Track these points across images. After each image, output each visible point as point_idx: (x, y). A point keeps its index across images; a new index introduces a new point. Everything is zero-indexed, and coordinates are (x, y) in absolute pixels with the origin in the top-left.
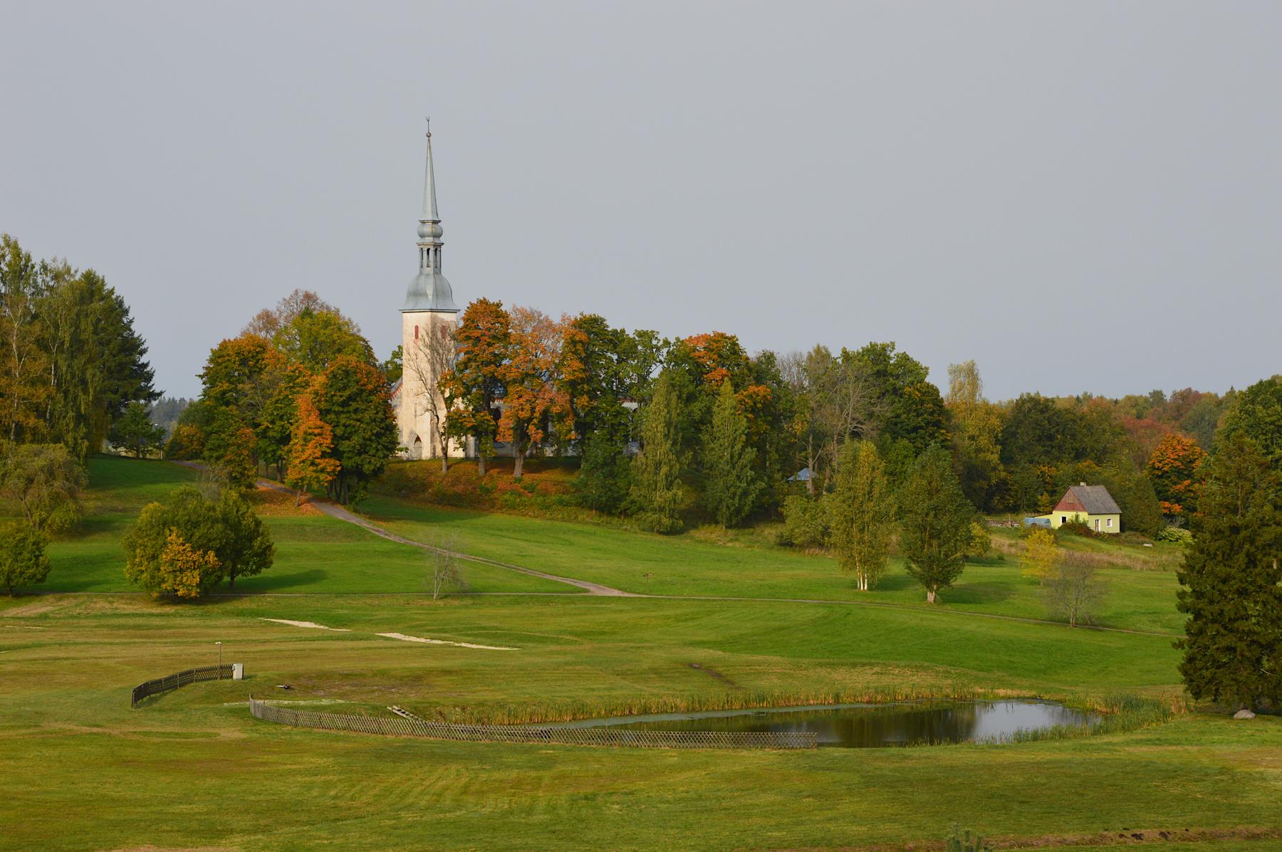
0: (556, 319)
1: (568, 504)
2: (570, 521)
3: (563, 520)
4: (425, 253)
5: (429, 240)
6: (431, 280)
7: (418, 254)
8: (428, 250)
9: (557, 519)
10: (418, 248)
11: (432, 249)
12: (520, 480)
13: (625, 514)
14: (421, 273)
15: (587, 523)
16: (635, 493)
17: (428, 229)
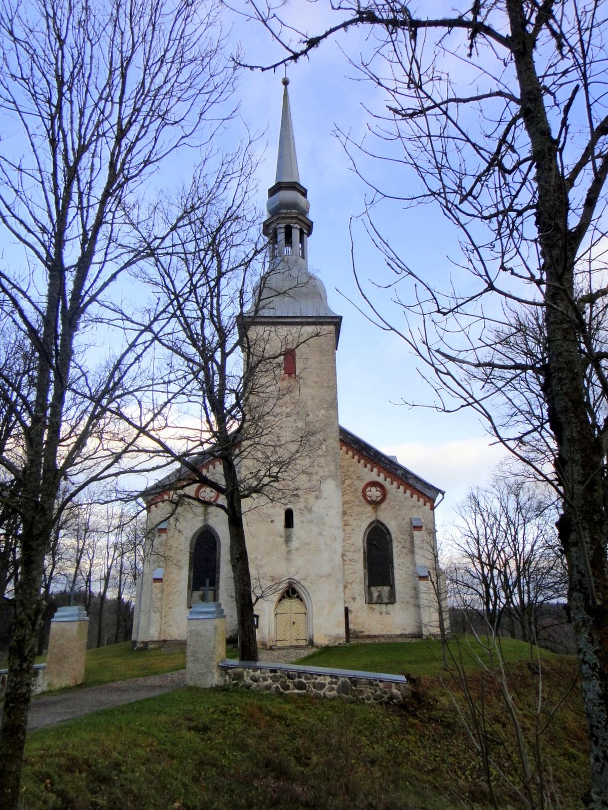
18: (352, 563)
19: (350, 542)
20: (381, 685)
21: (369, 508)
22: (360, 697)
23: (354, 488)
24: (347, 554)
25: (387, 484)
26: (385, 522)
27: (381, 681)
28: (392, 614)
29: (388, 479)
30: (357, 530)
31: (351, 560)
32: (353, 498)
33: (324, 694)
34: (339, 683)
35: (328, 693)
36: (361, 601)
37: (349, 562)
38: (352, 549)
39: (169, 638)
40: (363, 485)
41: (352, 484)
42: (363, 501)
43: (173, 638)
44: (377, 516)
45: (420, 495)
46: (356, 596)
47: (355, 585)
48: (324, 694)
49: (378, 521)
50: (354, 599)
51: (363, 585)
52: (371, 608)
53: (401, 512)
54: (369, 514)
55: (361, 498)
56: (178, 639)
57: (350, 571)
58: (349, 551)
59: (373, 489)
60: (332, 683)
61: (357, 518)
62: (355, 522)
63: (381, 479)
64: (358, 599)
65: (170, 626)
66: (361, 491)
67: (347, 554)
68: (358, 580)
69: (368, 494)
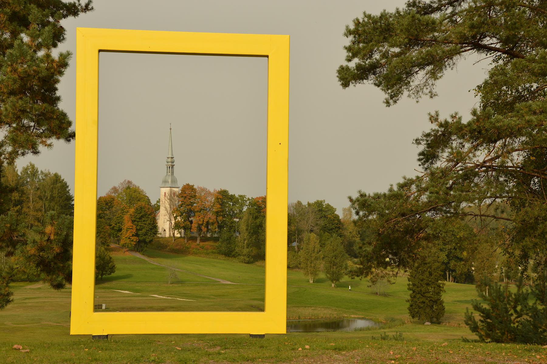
0: (212, 191)
1: (215, 253)
2: (215, 259)
3: (213, 258)
4: (168, 168)
5: (170, 164)
6: (170, 177)
7: (166, 168)
8: (170, 167)
9: (211, 258)
10: (166, 166)
11: (171, 167)
12: (199, 245)
13: (234, 256)
14: (167, 175)
15: (221, 259)
16: (237, 249)
17: (170, 160)
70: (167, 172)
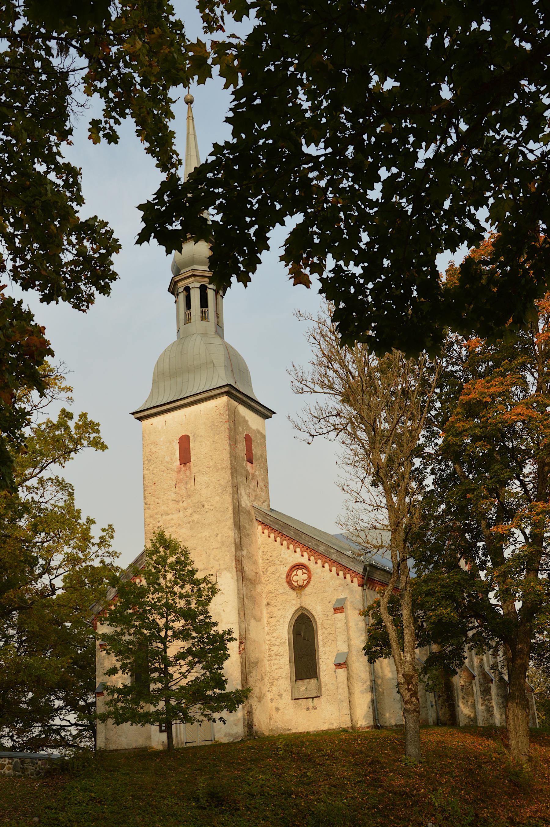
18: (278, 657)
19: (275, 635)
20: (39, 762)
21: (293, 594)
22: (27, 773)
23: (278, 574)
24: (273, 648)
25: (311, 565)
26: (310, 608)
27: (40, 760)
28: (318, 708)
29: (312, 558)
30: (281, 621)
31: (276, 655)
32: (277, 587)
33: (4, 772)
34: (13, 763)
35: (7, 772)
36: (287, 698)
37: (274, 657)
38: (277, 643)
39: (119, 748)
40: (287, 569)
41: (276, 571)
42: (288, 589)
43: (123, 747)
44: (301, 602)
45: (346, 571)
46: (282, 692)
47: (281, 681)
48: (4, 772)
49: (302, 608)
50: (280, 695)
51: (289, 680)
52: (297, 704)
53: (326, 594)
54: (294, 602)
55: (286, 585)
56: (127, 747)
57: (276, 667)
58: (274, 645)
59: (300, 572)
60: (9, 763)
61: (281, 607)
62: (280, 612)
63: (304, 560)
64: (285, 695)
65: (120, 736)
66: (284, 576)
67: (273, 648)
68: (284, 674)
69: (295, 578)
70: (188, 320)
